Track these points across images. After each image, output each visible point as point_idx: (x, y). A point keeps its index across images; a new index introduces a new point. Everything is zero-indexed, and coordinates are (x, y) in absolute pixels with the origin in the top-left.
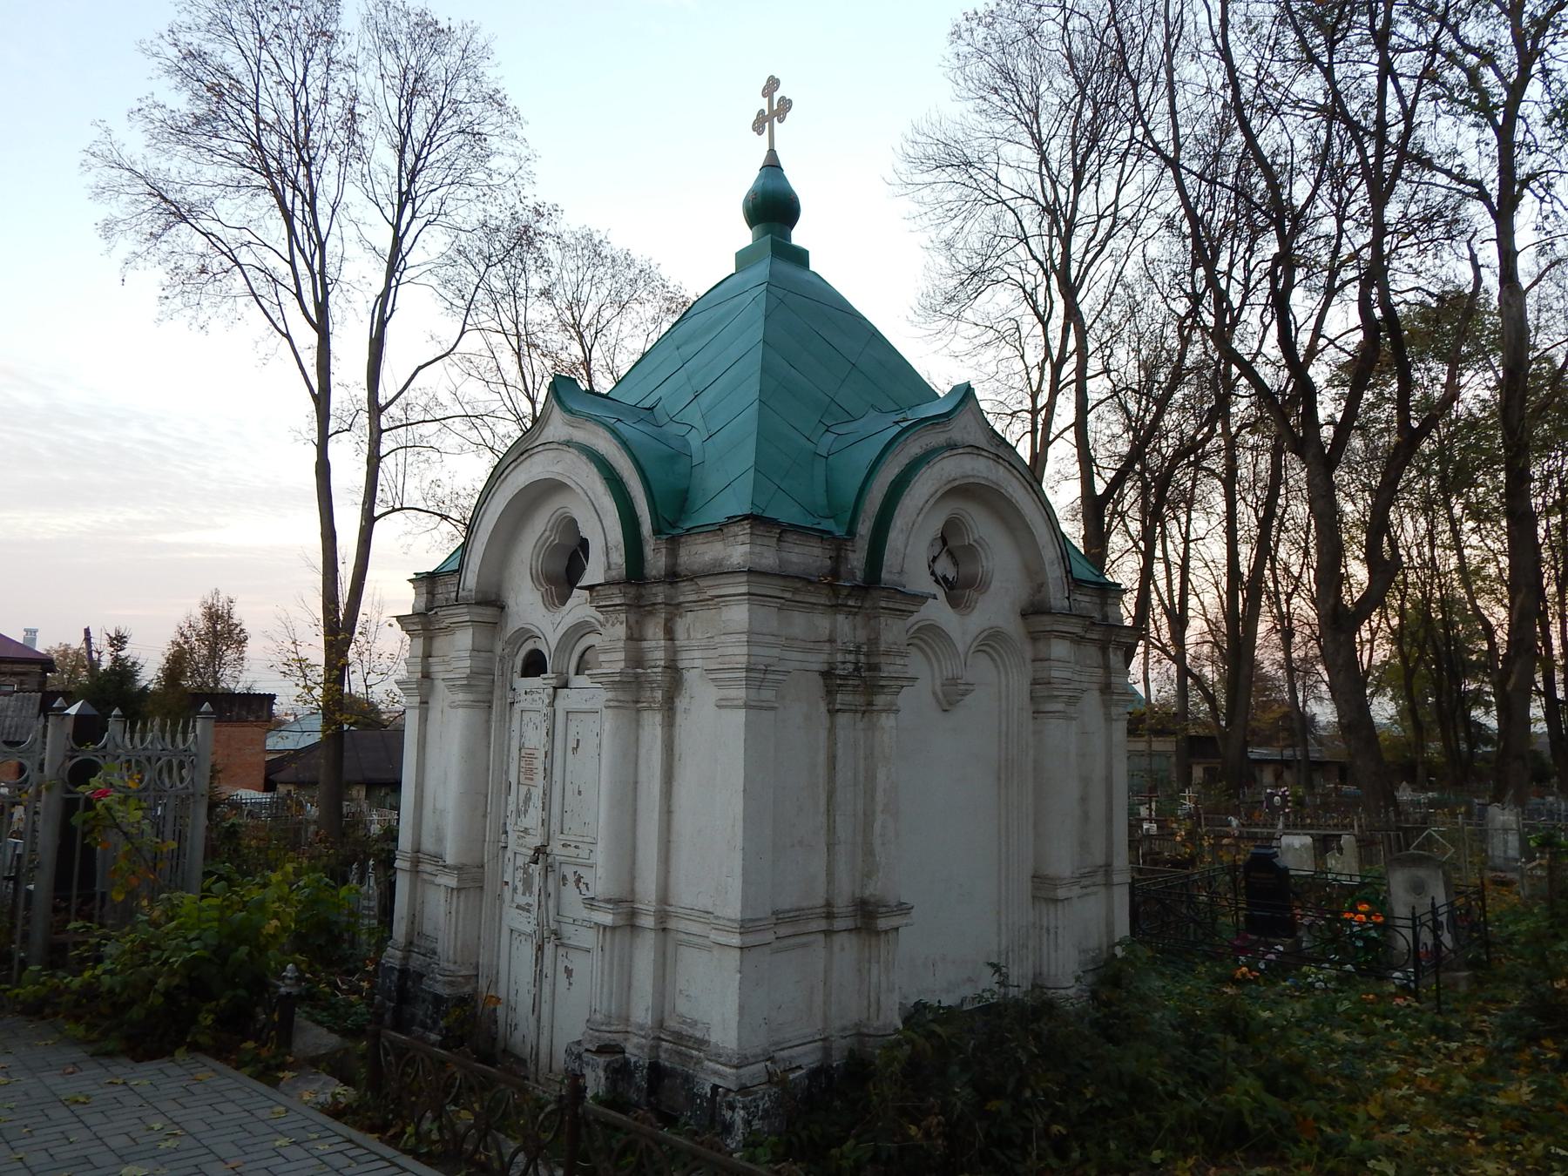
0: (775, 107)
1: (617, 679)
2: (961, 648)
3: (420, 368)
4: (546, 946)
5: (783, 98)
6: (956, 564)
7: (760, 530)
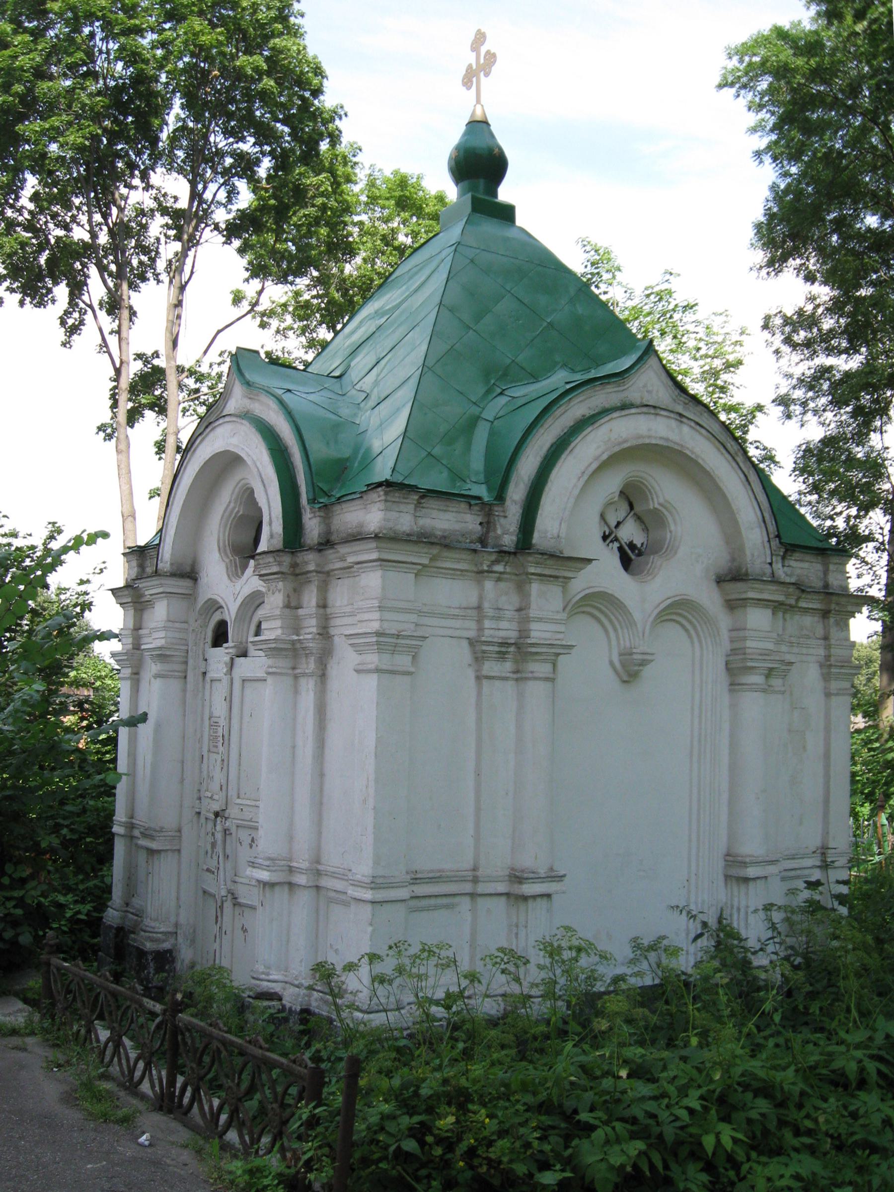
0: (482, 61)
1: (273, 645)
2: (637, 616)
3: (219, 332)
4: (225, 905)
5: (488, 52)
6: (646, 529)
7: (396, 496)
